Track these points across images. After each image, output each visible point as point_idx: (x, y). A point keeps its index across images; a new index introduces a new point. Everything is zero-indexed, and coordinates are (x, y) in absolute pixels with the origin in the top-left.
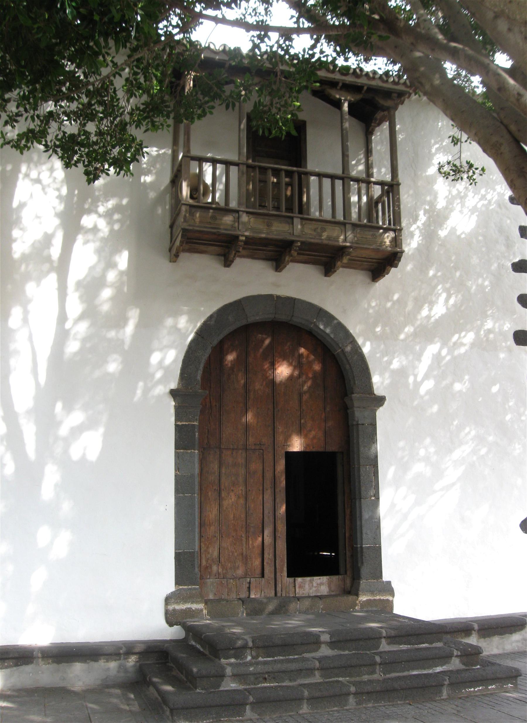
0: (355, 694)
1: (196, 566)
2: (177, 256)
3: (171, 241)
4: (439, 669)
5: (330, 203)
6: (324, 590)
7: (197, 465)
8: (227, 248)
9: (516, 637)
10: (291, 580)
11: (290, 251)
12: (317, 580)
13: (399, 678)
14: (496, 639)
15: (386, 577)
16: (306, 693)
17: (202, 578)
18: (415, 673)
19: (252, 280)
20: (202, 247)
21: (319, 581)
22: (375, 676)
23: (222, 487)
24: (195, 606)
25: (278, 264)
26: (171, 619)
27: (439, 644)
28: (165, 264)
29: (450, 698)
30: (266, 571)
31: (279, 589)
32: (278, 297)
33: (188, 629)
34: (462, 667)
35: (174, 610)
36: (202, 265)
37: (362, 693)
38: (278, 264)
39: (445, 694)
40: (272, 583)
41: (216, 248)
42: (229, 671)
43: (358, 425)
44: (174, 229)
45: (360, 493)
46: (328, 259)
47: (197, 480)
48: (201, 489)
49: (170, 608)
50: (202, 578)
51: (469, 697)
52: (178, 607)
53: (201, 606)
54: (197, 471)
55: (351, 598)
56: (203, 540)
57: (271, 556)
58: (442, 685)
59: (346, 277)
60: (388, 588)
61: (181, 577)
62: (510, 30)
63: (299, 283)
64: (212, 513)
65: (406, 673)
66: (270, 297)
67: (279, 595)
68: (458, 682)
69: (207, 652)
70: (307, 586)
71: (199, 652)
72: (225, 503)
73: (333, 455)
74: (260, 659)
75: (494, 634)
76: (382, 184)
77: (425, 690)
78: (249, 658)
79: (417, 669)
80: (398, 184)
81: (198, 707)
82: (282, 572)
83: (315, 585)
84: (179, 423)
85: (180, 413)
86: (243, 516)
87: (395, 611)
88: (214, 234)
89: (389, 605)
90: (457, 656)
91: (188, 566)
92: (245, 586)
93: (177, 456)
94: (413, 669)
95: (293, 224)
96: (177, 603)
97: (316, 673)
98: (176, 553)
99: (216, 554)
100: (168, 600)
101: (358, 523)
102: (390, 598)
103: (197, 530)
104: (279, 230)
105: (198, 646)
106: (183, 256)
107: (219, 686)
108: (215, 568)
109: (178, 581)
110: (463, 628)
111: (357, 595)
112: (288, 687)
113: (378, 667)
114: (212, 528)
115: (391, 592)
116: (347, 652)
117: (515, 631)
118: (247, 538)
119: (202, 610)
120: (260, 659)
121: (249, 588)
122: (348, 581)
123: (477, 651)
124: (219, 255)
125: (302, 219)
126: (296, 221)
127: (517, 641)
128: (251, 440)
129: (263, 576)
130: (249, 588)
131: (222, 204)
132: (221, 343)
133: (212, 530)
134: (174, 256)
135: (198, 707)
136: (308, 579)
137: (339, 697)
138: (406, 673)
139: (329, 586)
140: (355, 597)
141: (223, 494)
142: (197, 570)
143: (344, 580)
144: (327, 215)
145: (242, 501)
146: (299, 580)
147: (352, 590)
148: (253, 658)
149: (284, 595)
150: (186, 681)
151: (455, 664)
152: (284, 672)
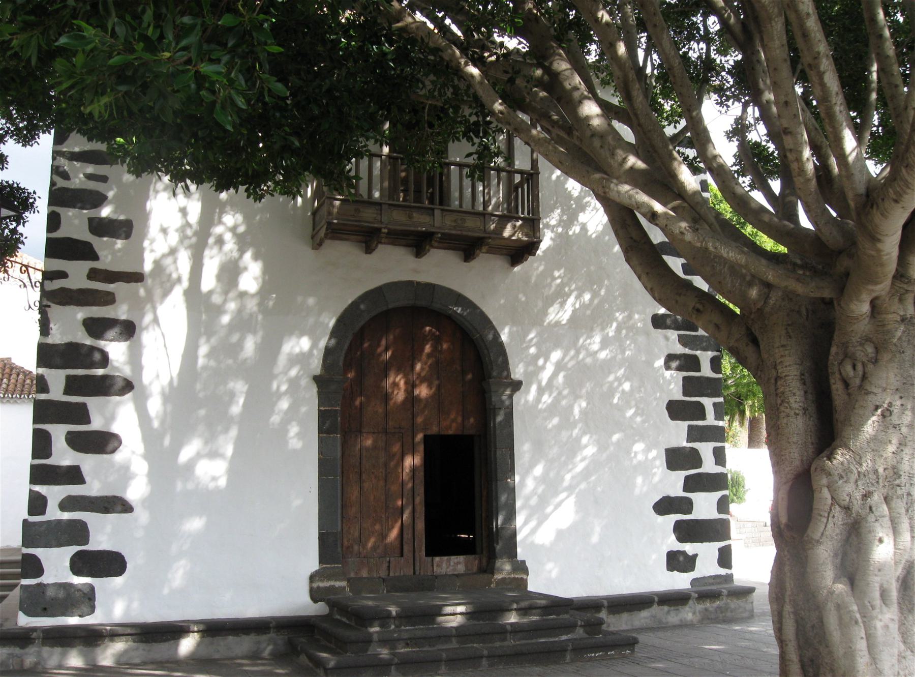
0: (488, 657)
1: (339, 545)
2: (320, 244)
3: (314, 229)
4: (564, 638)
5: (470, 190)
6: (461, 569)
7: (339, 449)
8: (369, 239)
9: (645, 614)
10: (429, 559)
11: (431, 241)
12: (454, 559)
13: (528, 644)
14: (625, 616)
15: (520, 557)
16: (444, 655)
17: (344, 557)
18: (543, 640)
19: (394, 266)
20: (344, 236)
21: (456, 561)
22: (506, 643)
23: (363, 470)
24: (338, 584)
25: (419, 252)
26: (316, 594)
27: (566, 616)
28: (306, 252)
29: (572, 661)
30: (406, 548)
31: (417, 568)
32: (418, 283)
33: (332, 604)
34: (586, 636)
35: (318, 587)
36: (344, 252)
37: (494, 656)
38: (419, 252)
39: (568, 657)
40: (411, 562)
41: (359, 237)
42: (375, 637)
43: (495, 409)
44: (317, 218)
45: (496, 475)
46: (469, 247)
47: (339, 462)
48: (342, 472)
49: (315, 585)
50: (344, 557)
51: (591, 659)
52: (322, 585)
53: (344, 584)
54: (339, 454)
55: (486, 576)
56: (344, 521)
57: (410, 536)
58: (566, 651)
59: (487, 264)
60: (522, 567)
61: (324, 557)
62: (601, 147)
63: (440, 269)
64: (354, 494)
65: (534, 641)
66: (410, 283)
67: (417, 573)
68: (580, 650)
69: (353, 624)
70: (444, 565)
71: (345, 623)
72: (366, 485)
73: (471, 437)
74: (403, 628)
75: (622, 611)
76: (521, 172)
77: (551, 655)
78: (393, 627)
79: (544, 637)
80: (538, 173)
81: (350, 667)
82: (420, 551)
83: (452, 564)
84: (322, 408)
85: (324, 396)
86: (383, 497)
87: (530, 588)
88: (357, 226)
89: (523, 583)
90: (581, 626)
91: (330, 546)
92: (385, 566)
93: (321, 440)
94: (541, 637)
95: (434, 215)
96: (322, 581)
97: (454, 640)
98: (319, 533)
99: (357, 534)
100: (312, 578)
101: (494, 504)
102: (525, 577)
103: (339, 511)
104: (421, 222)
105: (344, 620)
106: (328, 242)
107: (367, 650)
108: (356, 548)
109: (322, 560)
110: (591, 605)
111: (493, 574)
112: (428, 651)
113: (508, 635)
114: (354, 509)
115: (525, 571)
116: (481, 622)
117: (644, 609)
118: (387, 519)
119: (344, 588)
120: (403, 628)
121: (389, 567)
122: (484, 561)
123: (601, 622)
124: (361, 242)
125: (442, 210)
126: (437, 213)
127: (645, 618)
128: (391, 423)
129: (402, 555)
130: (389, 567)
131: (365, 196)
132: (362, 329)
133: (353, 511)
134: (317, 244)
135: (350, 667)
136: (446, 558)
137: (473, 660)
138: (534, 641)
139: (466, 566)
140: (490, 576)
141: (364, 476)
142: (339, 550)
143: (480, 561)
144: (467, 206)
145: (382, 483)
146: (437, 559)
147: (488, 568)
148: (396, 627)
149: (422, 573)
150: (338, 645)
151: (580, 633)
152: (424, 638)
